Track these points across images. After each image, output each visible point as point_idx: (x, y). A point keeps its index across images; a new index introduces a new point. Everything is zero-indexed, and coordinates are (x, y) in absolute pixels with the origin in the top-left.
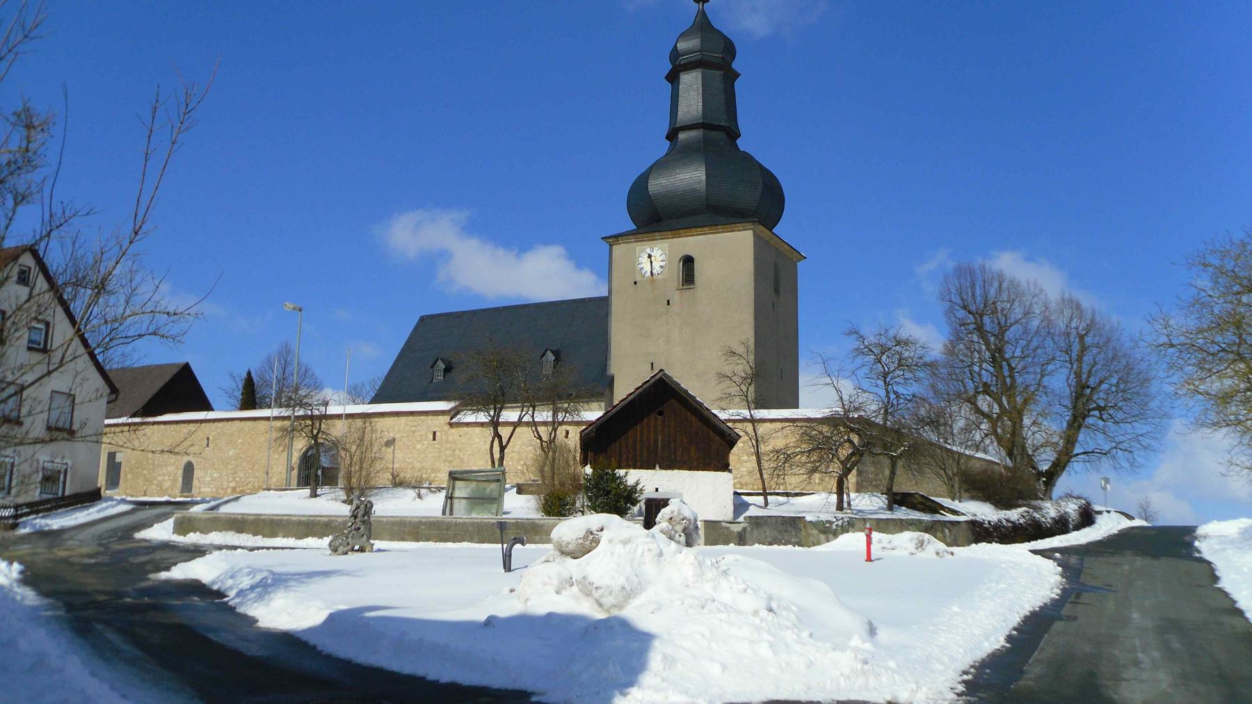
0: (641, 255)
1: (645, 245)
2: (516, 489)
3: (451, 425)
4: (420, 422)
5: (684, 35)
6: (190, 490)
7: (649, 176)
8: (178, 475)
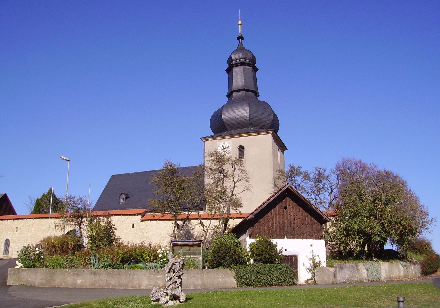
0: (219, 146)
1: (220, 141)
2: (278, 251)
3: (142, 221)
4: (126, 219)
5: (235, 52)
6: (8, 254)
7: (222, 110)
8: (2, 246)
